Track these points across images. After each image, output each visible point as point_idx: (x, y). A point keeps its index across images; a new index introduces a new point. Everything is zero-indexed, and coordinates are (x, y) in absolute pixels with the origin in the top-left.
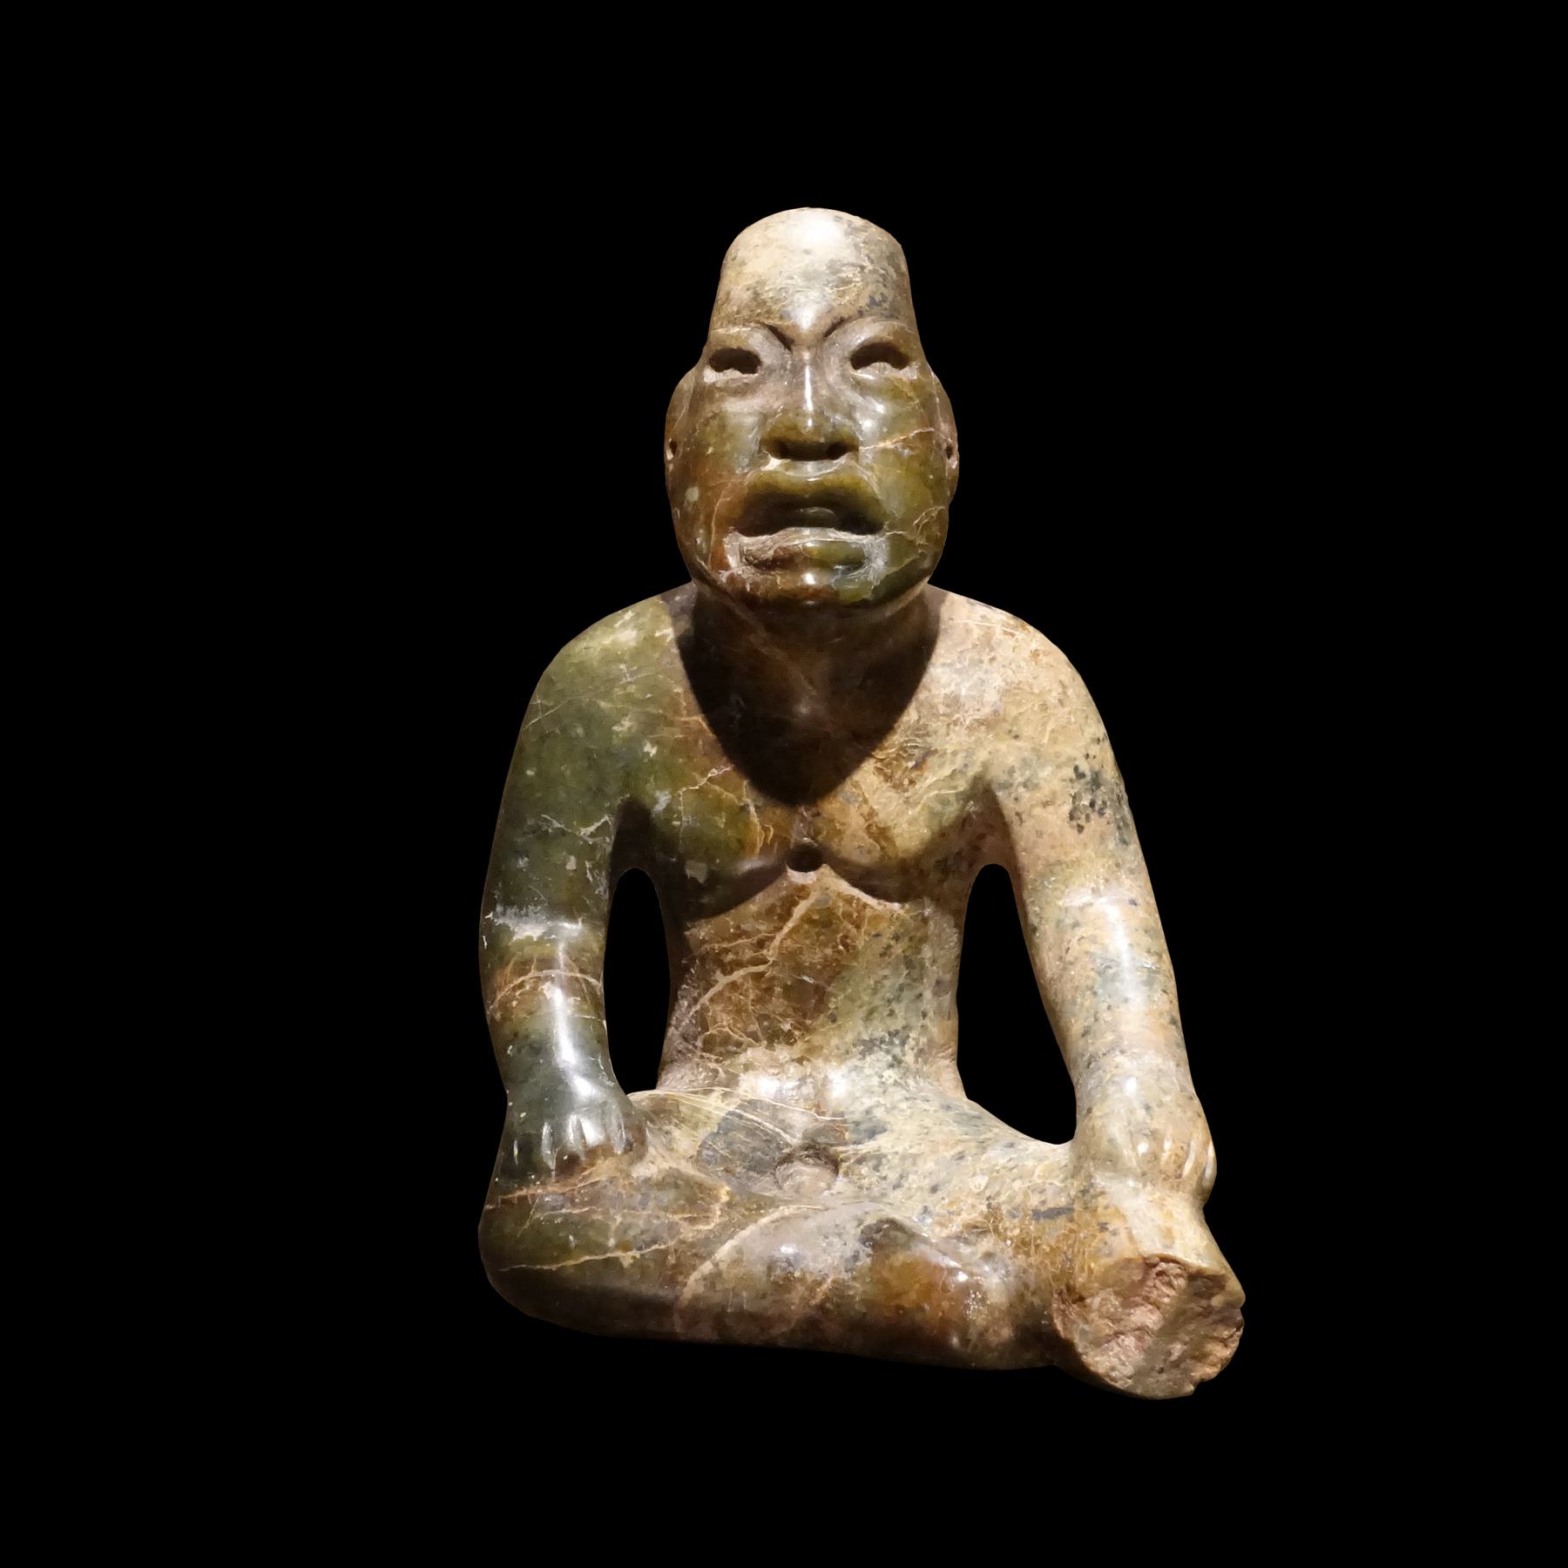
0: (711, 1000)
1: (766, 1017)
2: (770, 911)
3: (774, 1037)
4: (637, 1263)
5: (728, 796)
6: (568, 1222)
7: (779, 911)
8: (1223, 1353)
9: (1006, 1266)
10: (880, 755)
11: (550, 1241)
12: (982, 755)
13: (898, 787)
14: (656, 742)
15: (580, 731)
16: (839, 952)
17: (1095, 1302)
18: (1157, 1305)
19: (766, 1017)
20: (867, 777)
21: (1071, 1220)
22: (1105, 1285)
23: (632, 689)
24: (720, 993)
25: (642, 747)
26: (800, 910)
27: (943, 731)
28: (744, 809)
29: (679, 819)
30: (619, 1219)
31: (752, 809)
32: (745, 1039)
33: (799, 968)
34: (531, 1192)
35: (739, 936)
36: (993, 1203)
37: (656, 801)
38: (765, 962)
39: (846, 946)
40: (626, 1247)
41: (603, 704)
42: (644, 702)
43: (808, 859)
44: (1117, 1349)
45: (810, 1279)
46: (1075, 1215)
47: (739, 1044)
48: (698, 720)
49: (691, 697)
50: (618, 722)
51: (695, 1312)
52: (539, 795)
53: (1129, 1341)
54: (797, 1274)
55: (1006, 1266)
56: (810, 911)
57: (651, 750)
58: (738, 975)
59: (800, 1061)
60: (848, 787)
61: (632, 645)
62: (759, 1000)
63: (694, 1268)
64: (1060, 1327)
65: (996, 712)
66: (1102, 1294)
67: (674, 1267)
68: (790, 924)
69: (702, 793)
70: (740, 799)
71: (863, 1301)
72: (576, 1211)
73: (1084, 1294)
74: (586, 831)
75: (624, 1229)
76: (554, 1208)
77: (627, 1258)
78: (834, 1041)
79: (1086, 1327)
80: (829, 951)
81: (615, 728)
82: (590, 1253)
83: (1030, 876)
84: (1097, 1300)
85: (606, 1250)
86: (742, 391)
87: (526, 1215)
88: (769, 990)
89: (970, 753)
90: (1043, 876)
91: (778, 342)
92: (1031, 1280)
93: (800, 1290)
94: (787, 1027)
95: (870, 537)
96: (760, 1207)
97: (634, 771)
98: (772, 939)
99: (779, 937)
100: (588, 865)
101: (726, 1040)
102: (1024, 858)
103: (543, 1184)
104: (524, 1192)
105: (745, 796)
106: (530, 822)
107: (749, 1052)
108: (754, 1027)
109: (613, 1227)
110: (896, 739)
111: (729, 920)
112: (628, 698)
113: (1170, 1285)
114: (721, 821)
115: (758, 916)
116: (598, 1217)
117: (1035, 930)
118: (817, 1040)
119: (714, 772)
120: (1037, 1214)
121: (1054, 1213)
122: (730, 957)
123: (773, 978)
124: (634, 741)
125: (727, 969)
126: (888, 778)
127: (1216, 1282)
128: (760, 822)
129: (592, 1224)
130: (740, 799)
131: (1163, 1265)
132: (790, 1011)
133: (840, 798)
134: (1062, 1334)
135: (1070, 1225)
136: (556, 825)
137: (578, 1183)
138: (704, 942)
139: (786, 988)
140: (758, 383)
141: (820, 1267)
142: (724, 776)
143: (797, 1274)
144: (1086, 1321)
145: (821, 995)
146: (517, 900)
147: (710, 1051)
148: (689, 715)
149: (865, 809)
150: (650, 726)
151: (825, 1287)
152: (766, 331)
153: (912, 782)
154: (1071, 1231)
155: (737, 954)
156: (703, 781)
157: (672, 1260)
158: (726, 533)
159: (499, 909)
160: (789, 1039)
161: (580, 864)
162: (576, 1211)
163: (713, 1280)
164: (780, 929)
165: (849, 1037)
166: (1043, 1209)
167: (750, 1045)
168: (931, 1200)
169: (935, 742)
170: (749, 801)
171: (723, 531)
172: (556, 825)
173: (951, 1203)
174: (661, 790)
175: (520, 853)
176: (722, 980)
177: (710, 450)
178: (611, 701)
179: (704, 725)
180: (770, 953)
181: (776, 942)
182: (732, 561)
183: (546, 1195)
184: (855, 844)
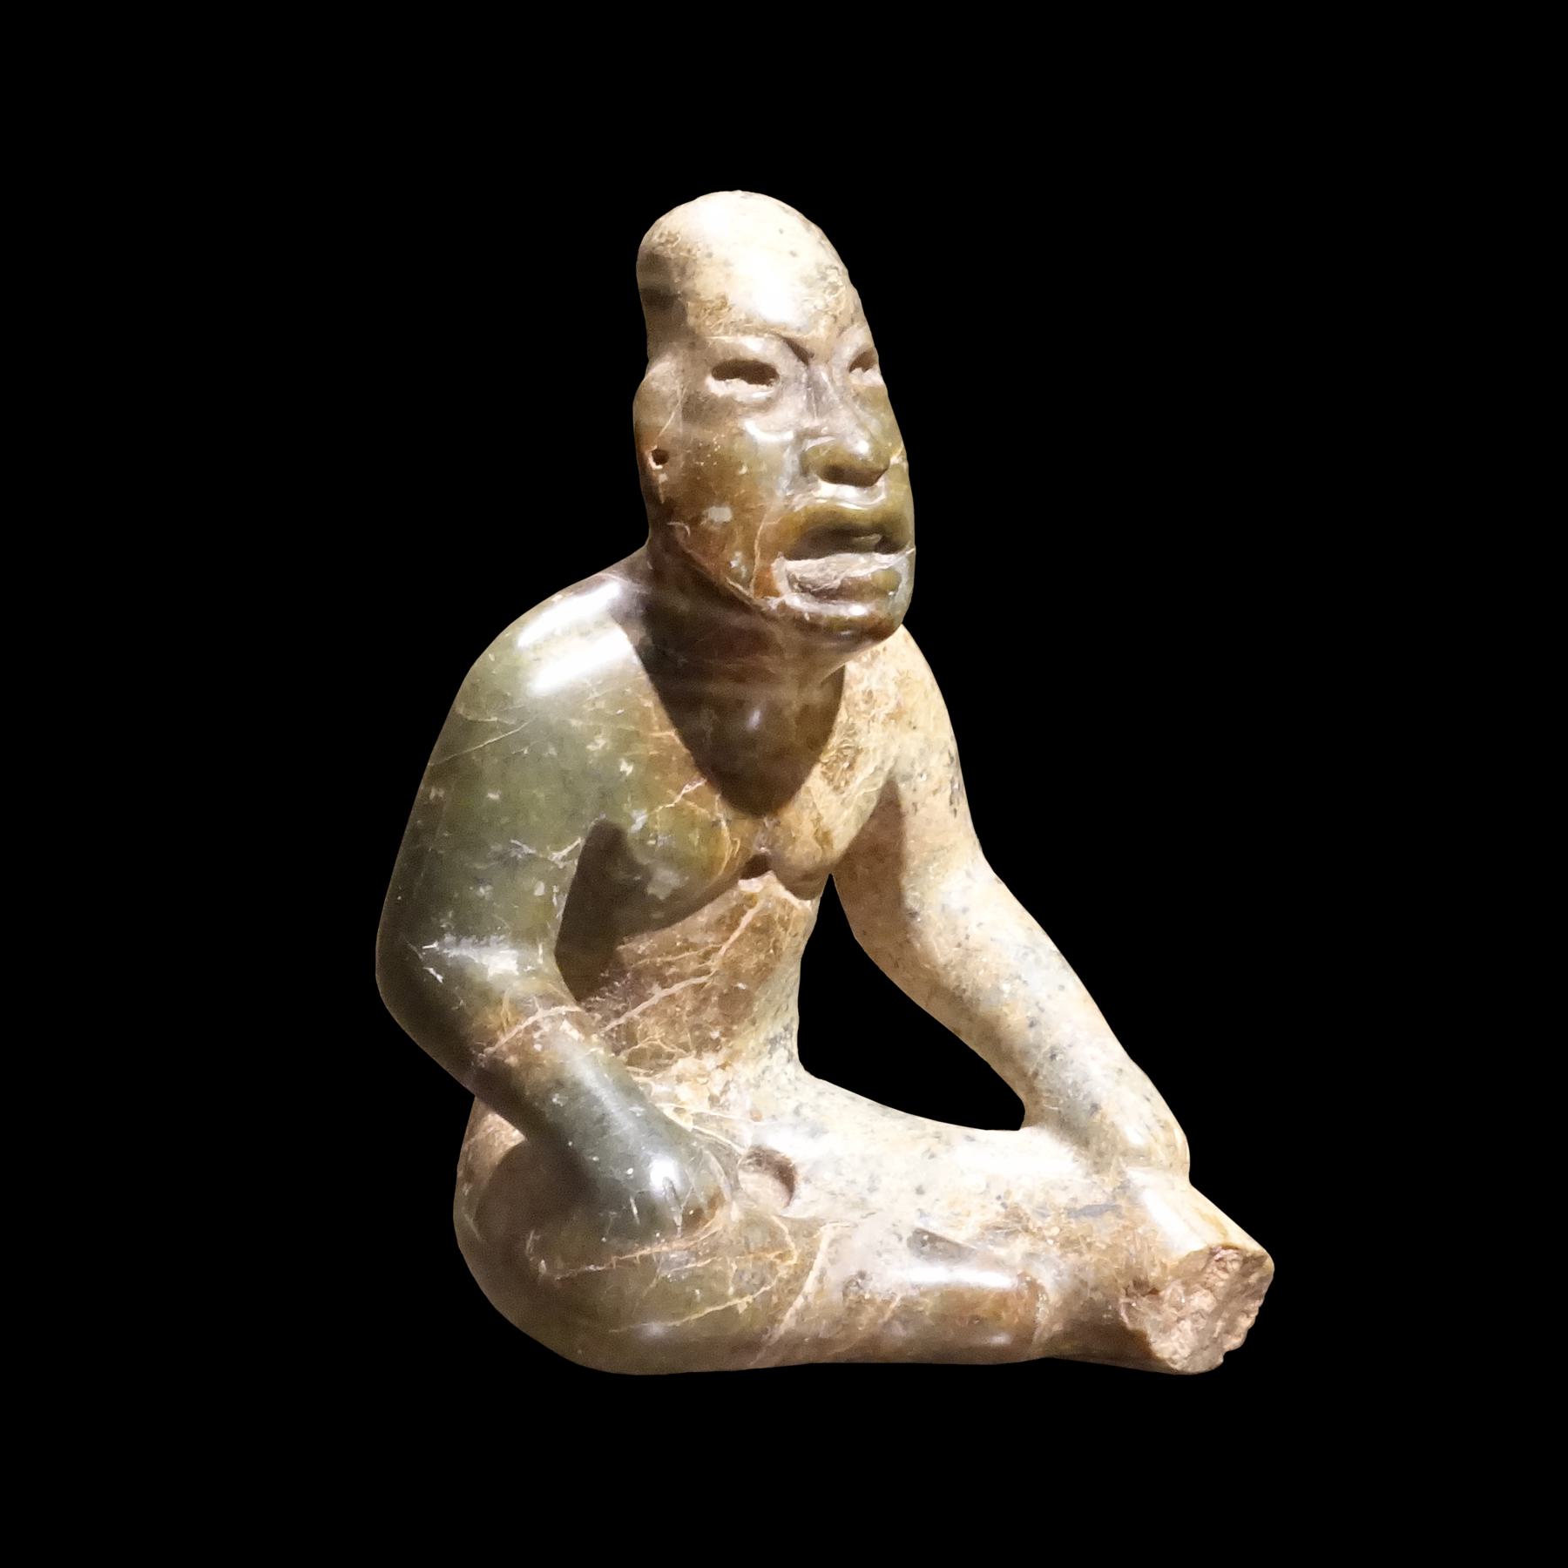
0: (643, 1014)
1: (699, 1027)
2: (720, 921)
3: (704, 1045)
4: (751, 1308)
5: (702, 812)
6: (695, 1277)
7: (728, 921)
8: (1246, 1323)
9: (1057, 1266)
10: (824, 758)
11: (674, 1298)
12: (894, 750)
13: (836, 788)
14: (630, 760)
15: (552, 751)
16: (769, 956)
17: (1166, 1293)
18: (1211, 1289)
19: (699, 1027)
20: (815, 782)
21: (1120, 1216)
22: (1177, 1277)
23: (601, 705)
24: (654, 1007)
25: (618, 765)
26: (745, 921)
27: (865, 728)
28: (716, 824)
29: (656, 838)
30: (735, 1267)
31: (724, 823)
32: (677, 1050)
33: (736, 976)
34: (656, 1249)
35: (681, 950)
36: (1008, 1202)
37: (633, 822)
38: (707, 972)
39: (775, 948)
40: (740, 1294)
41: (574, 722)
42: (614, 719)
43: (756, 867)
44: (1178, 1334)
45: (879, 1299)
46: (1124, 1212)
47: (670, 1056)
48: (671, 735)
49: (662, 712)
50: (592, 741)
51: (793, 1341)
52: (505, 820)
53: (1187, 1325)
54: (867, 1296)
55: (1057, 1266)
56: (755, 918)
57: (627, 768)
58: (677, 988)
59: (723, 1067)
60: (802, 795)
61: (572, 649)
62: (696, 1011)
63: (790, 1304)
64: (1126, 1320)
65: (898, 705)
66: (1173, 1285)
67: (776, 1305)
68: (736, 934)
69: (674, 811)
70: (712, 813)
71: (932, 1316)
72: (700, 1264)
73: (1158, 1286)
74: (557, 856)
75: (740, 1274)
76: (680, 1264)
77: (742, 1304)
78: (752, 1043)
79: (1159, 1318)
80: (762, 957)
81: (590, 747)
82: (714, 1303)
83: (913, 864)
84: (1169, 1292)
85: (725, 1298)
86: (765, 406)
87: (653, 1274)
88: (705, 1000)
89: (886, 748)
90: (927, 862)
91: (791, 354)
92: (1090, 1277)
93: (871, 1310)
94: (715, 1034)
95: (892, 556)
96: (810, 1234)
97: (610, 791)
98: (716, 950)
99: (724, 948)
100: (556, 890)
101: (657, 1054)
102: (911, 845)
103: (668, 1241)
104: (647, 1251)
105: (717, 810)
106: (497, 848)
107: (681, 1062)
108: (686, 1037)
109: (731, 1274)
110: (835, 741)
111: (675, 932)
112: (598, 714)
113: (1225, 1270)
114: (695, 837)
115: (707, 929)
116: (718, 1268)
117: (914, 915)
118: (737, 1043)
119: (688, 789)
120: (1072, 1213)
121: (1094, 1211)
122: (673, 970)
123: (713, 988)
124: (611, 758)
125: (664, 982)
126: (831, 781)
127: (1257, 1261)
128: (731, 835)
129: (714, 1276)
130: (712, 813)
131: (1224, 1252)
132: (721, 1019)
133: (797, 806)
134: (1130, 1326)
135: (1122, 1222)
136: (528, 850)
137: (701, 1235)
138: (642, 956)
139: (722, 997)
140: (779, 395)
141: (887, 1286)
142: (697, 793)
143: (867, 1296)
144: (1159, 1312)
145: (748, 999)
146: (473, 927)
147: (639, 1065)
148: (661, 729)
149: (815, 815)
150: (624, 742)
151: (893, 1306)
152: (780, 343)
153: (847, 783)
154: (1125, 1227)
155: (681, 966)
156: (678, 799)
157: (775, 1299)
158: (774, 556)
159: (448, 938)
160: (715, 1046)
161: (549, 888)
162: (700, 1264)
163: (801, 1315)
164: (726, 939)
165: (762, 1039)
166: (1078, 1207)
167: (681, 1056)
168: (923, 1202)
169: (861, 741)
170: (720, 815)
171: (771, 552)
172: (528, 850)
173: (952, 1204)
174: (635, 807)
175: (479, 882)
176: (658, 993)
177: (744, 470)
178: (581, 717)
179: (678, 741)
180: (714, 964)
181: (722, 952)
182: (782, 585)
183: (670, 1253)
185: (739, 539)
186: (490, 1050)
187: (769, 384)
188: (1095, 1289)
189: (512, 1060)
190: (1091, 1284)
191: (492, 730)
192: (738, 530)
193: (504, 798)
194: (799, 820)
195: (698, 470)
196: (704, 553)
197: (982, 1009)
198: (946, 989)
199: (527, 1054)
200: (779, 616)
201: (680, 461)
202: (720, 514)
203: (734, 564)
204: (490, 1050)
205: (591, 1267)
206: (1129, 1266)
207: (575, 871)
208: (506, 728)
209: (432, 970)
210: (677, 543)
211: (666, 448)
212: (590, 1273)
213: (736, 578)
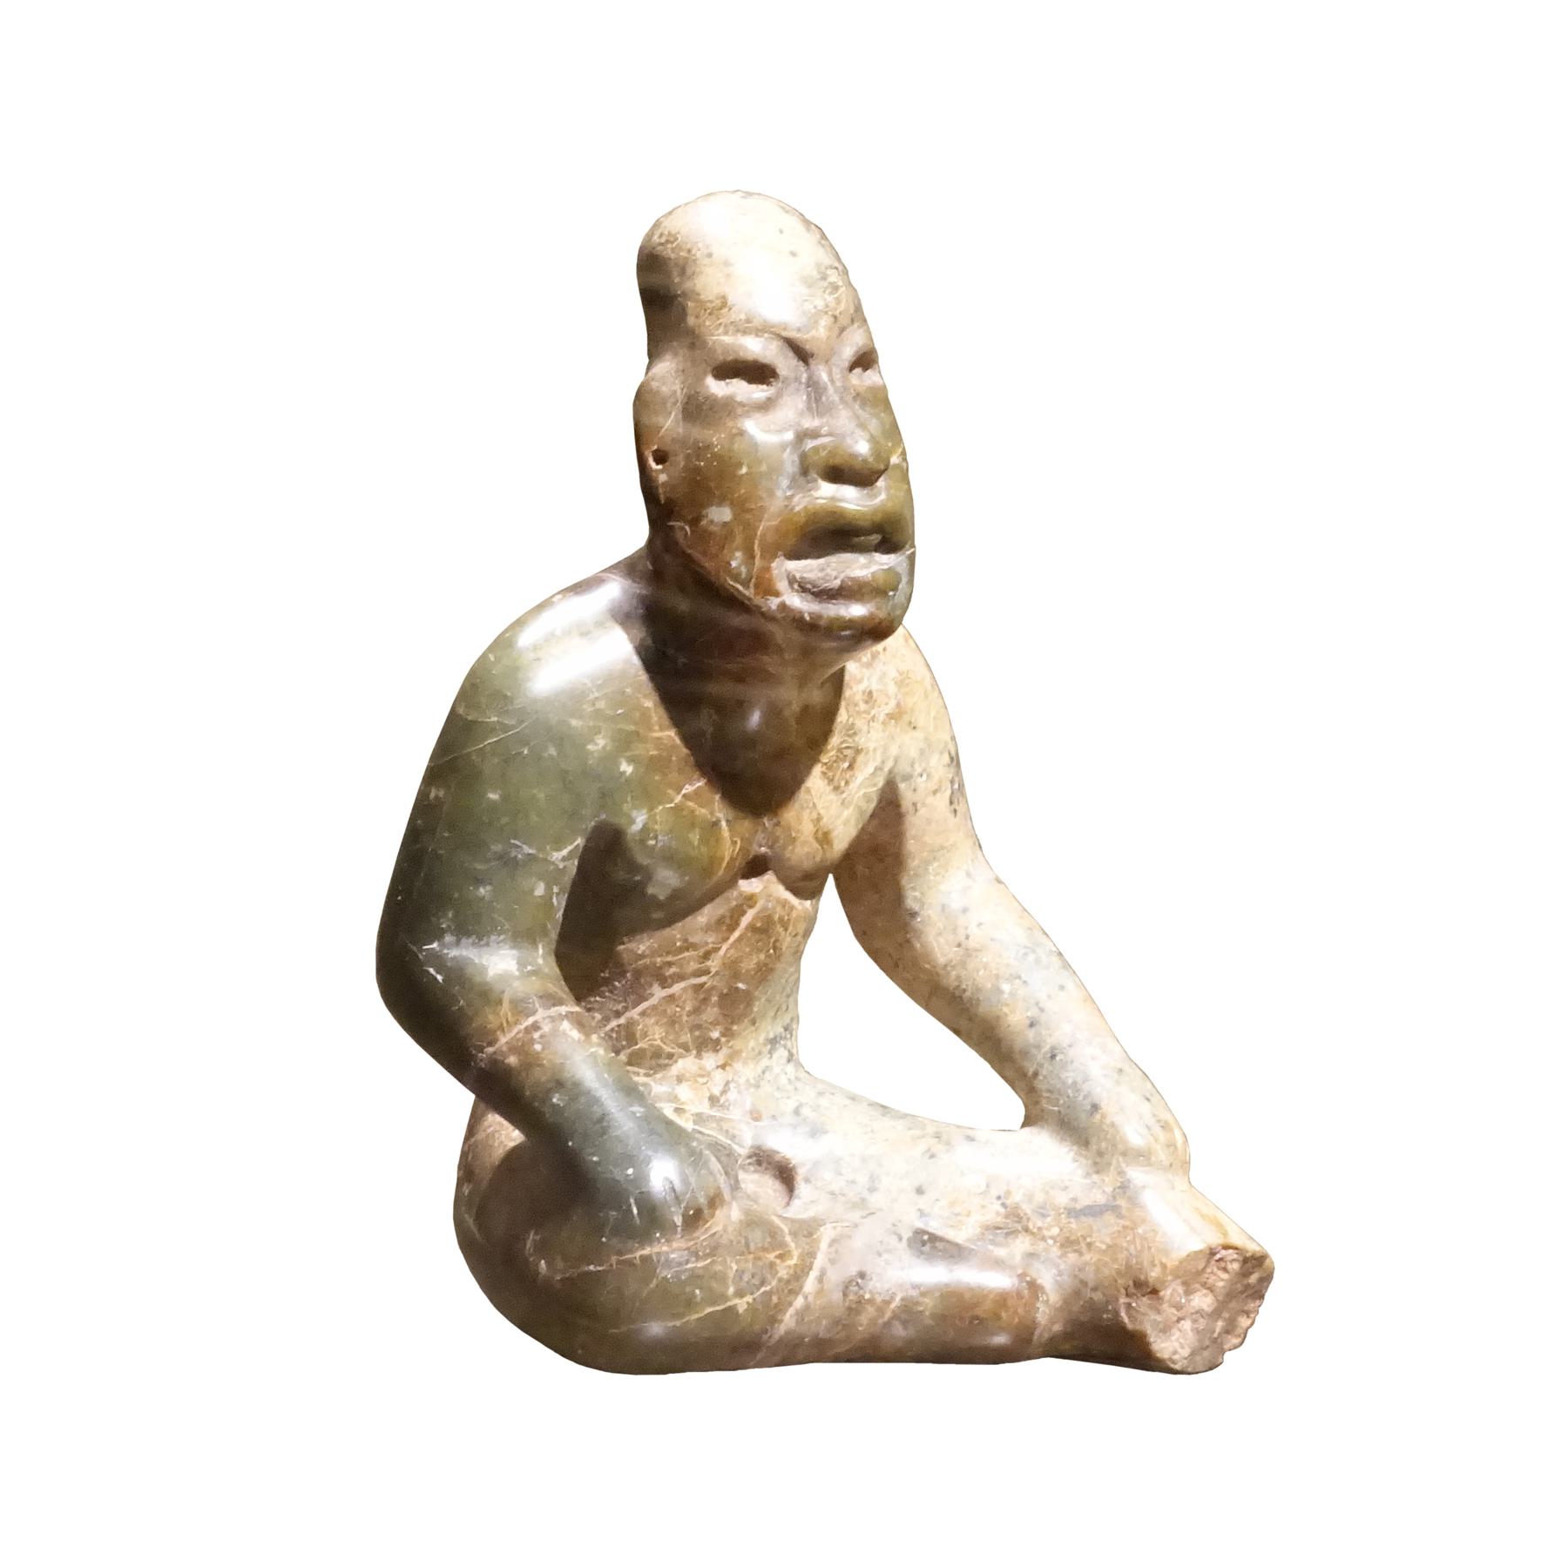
0: (643, 1014)
1: (699, 1027)
2: (720, 921)
3: (704, 1045)
4: (751, 1308)
5: (702, 812)
6: (695, 1277)
7: (728, 921)
9: (1057, 1266)
10: (824, 758)
12: (894, 750)
13: (836, 788)
14: (630, 760)
15: (552, 751)
16: (769, 956)
17: (1166, 1293)
18: (1211, 1289)
19: (699, 1027)
20: (815, 782)
21: (1120, 1216)
22: (1177, 1277)
23: (601, 705)
24: (654, 1007)
25: (618, 765)
26: (745, 921)
27: (865, 728)
28: (716, 824)
29: (656, 838)
30: (735, 1267)
31: (724, 823)
32: (677, 1050)
33: (736, 976)
34: (656, 1249)
35: (681, 950)
36: (1008, 1202)
37: (633, 822)
38: (707, 972)
39: (775, 948)
40: (740, 1294)
41: (574, 722)
42: (614, 719)
43: (756, 867)
44: (1178, 1334)
45: (879, 1299)
46: (1124, 1212)
47: (670, 1056)
48: (671, 735)
49: (662, 712)
50: (592, 741)
52: (505, 820)
53: (1187, 1325)
54: (867, 1296)
55: (1057, 1266)
56: (755, 918)
57: (627, 768)
58: (677, 988)
59: (723, 1067)
60: (802, 795)
62: (696, 1011)
63: (790, 1304)
64: (1126, 1320)
65: (898, 705)
66: (1173, 1285)
67: (776, 1305)
68: (736, 934)
70: (712, 813)
71: (932, 1316)
72: (700, 1264)
73: (1158, 1286)
74: (557, 856)
75: (740, 1274)
76: (680, 1264)
77: (742, 1304)
78: (752, 1043)
79: (1159, 1318)
80: (762, 957)
81: (590, 747)
82: (714, 1303)
83: (913, 864)
84: (1169, 1292)
85: (725, 1298)
86: (765, 406)
87: (653, 1274)
88: (705, 1000)
89: (886, 748)
90: (927, 862)
92: (1090, 1277)
93: (871, 1310)
94: (715, 1034)
95: (892, 556)
96: (810, 1234)
97: (610, 791)
98: (716, 950)
99: (724, 948)
100: (556, 890)
101: (657, 1054)
102: (911, 845)
103: (668, 1241)
104: (647, 1251)
105: (717, 810)
106: (497, 848)
107: (681, 1062)
108: (686, 1037)
109: (731, 1274)
110: (835, 741)
111: (675, 932)
112: (598, 714)
113: (1225, 1270)
114: (695, 837)
115: (707, 929)
116: (718, 1268)
117: (914, 915)
118: (737, 1043)
119: (688, 789)
120: (1072, 1213)
121: (1094, 1211)
122: (673, 970)
123: (713, 988)
124: (611, 758)
125: (664, 982)
126: (831, 781)
128: (731, 835)
129: (714, 1276)
130: (712, 813)
131: (1224, 1252)
132: (721, 1019)
133: (797, 806)
134: (1130, 1326)
135: (1122, 1222)
136: (528, 850)
137: (701, 1235)
138: (642, 956)
139: (722, 997)
140: (779, 395)
141: (887, 1286)
142: (697, 793)
143: (867, 1296)
144: (1159, 1312)
145: (748, 999)
147: (639, 1065)
148: (661, 729)
149: (815, 815)
150: (624, 742)
151: (893, 1306)
152: (780, 343)
153: (847, 783)
154: (1125, 1227)
155: (681, 966)
156: (678, 799)
157: (775, 1299)
158: (774, 556)
159: (448, 938)
160: (715, 1046)
161: (549, 888)
162: (700, 1264)
163: (801, 1315)
164: (726, 939)
165: (762, 1039)
166: (1078, 1207)
167: (681, 1056)
168: (923, 1202)
169: (861, 741)
170: (720, 815)
171: (771, 552)
172: (528, 850)
173: (952, 1204)
174: (635, 807)
175: (479, 882)
176: (658, 993)
177: (744, 470)
178: (581, 717)
179: (678, 741)
180: (714, 964)
181: (722, 952)
182: (782, 585)
183: (670, 1253)
184: (803, 851)
185: (739, 539)
186: (490, 1050)
187: (769, 384)
188: (1095, 1289)
189: (512, 1060)
190: (1091, 1284)
191: (492, 730)
192: (738, 530)
193: (504, 798)
194: (799, 820)
195: (698, 470)
196: (704, 553)
197: (982, 1009)
198: (946, 989)
199: (527, 1054)
200: (779, 616)
201: (680, 461)
202: (720, 514)
203: (734, 564)
204: (490, 1050)
205: (591, 1267)
206: (1129, 1266)
207: (575, 871)
208: (506, 728)
209: (432, 970)
210: (677, 543)
211: (666, 448)
212: (590, 1273)
213: (736, 578)
